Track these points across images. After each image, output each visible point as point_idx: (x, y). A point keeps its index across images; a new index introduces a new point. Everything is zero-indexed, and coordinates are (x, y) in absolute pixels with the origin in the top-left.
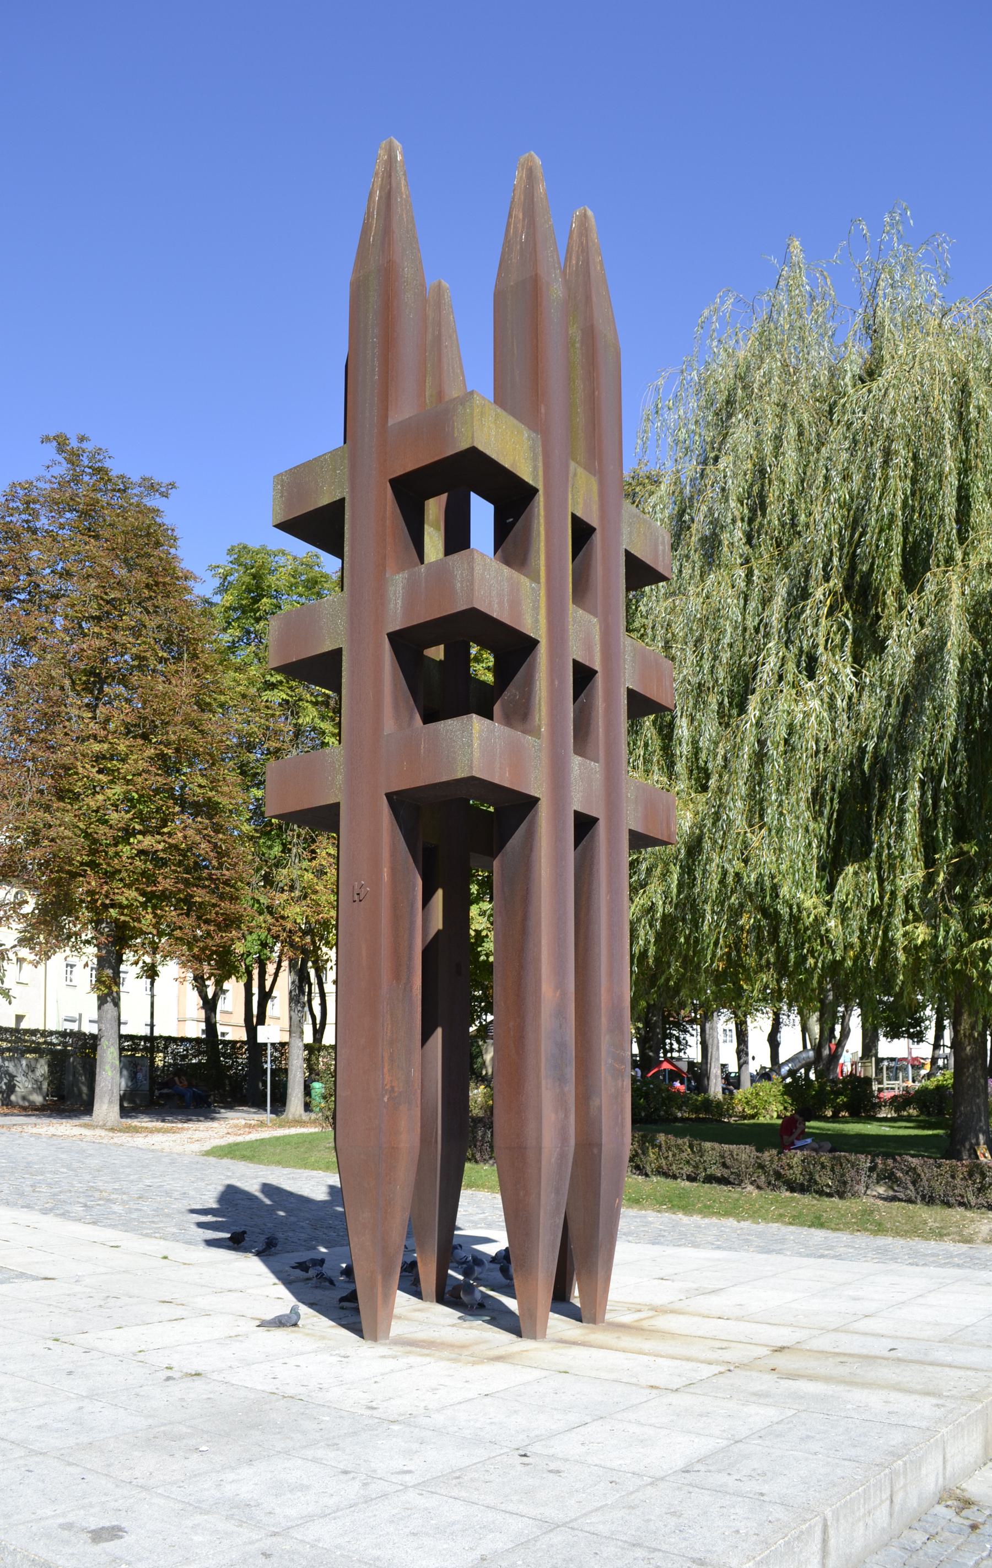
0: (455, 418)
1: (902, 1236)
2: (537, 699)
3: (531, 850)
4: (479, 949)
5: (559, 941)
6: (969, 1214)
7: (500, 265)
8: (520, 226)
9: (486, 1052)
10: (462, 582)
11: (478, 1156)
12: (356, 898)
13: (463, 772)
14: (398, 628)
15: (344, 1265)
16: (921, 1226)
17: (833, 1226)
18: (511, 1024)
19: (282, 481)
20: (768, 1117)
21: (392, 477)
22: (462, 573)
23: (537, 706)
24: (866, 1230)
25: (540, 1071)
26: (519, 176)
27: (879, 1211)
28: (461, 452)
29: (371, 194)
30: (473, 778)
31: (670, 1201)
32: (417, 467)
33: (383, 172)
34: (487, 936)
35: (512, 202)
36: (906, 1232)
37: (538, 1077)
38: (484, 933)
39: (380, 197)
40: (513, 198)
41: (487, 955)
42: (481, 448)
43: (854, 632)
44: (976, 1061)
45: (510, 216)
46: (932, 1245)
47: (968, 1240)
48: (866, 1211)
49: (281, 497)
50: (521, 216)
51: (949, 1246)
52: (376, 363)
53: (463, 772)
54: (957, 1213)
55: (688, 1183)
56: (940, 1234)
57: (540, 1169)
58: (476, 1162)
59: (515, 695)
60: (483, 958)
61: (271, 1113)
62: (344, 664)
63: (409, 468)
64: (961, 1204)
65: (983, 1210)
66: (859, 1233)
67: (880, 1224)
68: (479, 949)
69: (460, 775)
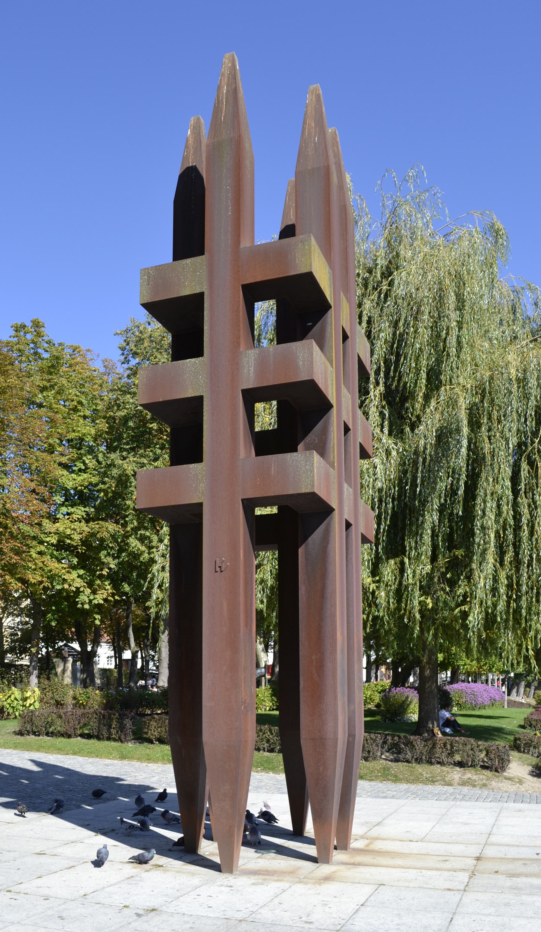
0: (296, 250)
1: (411, 783)
2: (332, 444)
3: (328, 543)
4: (77, 600)
5: (342, 602)
6: (444, 768)
7: (299, 155)
8: (313, 131)
9: (58, 667)
10: (303, 361)
11: (123, 737)
12: (218, 569)
13: (306, 489)
14: (251, 387)
15: (119, 818)
16: (420, 777)
17: (368, 778)
18: (314, 657)
19: (149, 273)
20: (263, 710)
21: (244, 283)
22: (303, 356)
23: (332, 449)
24: (389, 780)
25: (336, 688)
26: (309, 98)
27: (392, 768)
28: (301, 274)
29: (219, 88)
30: (314, 494)
31: (263, 765)
32: (265, 279)
33: (229, 75)
34: (83, 592)
35: (305, 114)
36: (413, 780)
37: (335, 692)
38: (82, 589)
39: (227, 91)
40: (307, 111)
41: (83, 604)
42: (314, 274)
43: (390, 418)
44: (433, 678)
45: (304, 123)
46: (429, 788)
47: (450, 784)
48: (384, 768)
49: (148, 284)
50: (313, 125)
51: (438, 788)
52: (230, 204)
53: (306, 489)
54: (437, 768)
55: (268, 753)
56: (433, 781)
57: (336, 752)
58: (122, 742)
59: (315, 440)
60: (79, 606)
61: (365, 722)
62: (205, 407)
63: (259, 279)
64: (439, 763)
65: (451, 766)
66: (385, 782)
67: (396, 776)
68: (77, 600)
69: (304, 490)
